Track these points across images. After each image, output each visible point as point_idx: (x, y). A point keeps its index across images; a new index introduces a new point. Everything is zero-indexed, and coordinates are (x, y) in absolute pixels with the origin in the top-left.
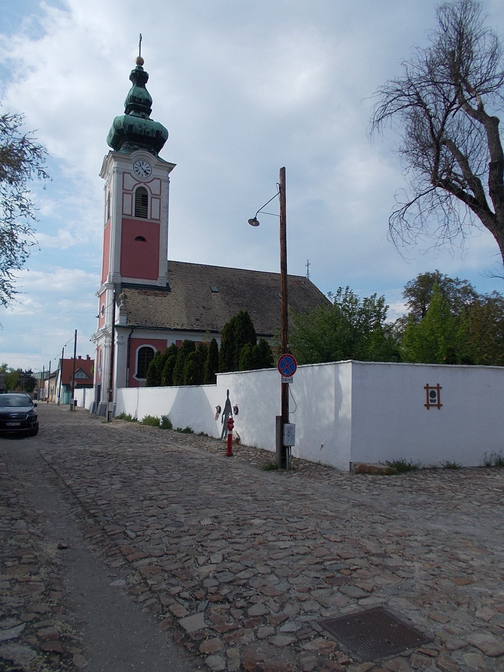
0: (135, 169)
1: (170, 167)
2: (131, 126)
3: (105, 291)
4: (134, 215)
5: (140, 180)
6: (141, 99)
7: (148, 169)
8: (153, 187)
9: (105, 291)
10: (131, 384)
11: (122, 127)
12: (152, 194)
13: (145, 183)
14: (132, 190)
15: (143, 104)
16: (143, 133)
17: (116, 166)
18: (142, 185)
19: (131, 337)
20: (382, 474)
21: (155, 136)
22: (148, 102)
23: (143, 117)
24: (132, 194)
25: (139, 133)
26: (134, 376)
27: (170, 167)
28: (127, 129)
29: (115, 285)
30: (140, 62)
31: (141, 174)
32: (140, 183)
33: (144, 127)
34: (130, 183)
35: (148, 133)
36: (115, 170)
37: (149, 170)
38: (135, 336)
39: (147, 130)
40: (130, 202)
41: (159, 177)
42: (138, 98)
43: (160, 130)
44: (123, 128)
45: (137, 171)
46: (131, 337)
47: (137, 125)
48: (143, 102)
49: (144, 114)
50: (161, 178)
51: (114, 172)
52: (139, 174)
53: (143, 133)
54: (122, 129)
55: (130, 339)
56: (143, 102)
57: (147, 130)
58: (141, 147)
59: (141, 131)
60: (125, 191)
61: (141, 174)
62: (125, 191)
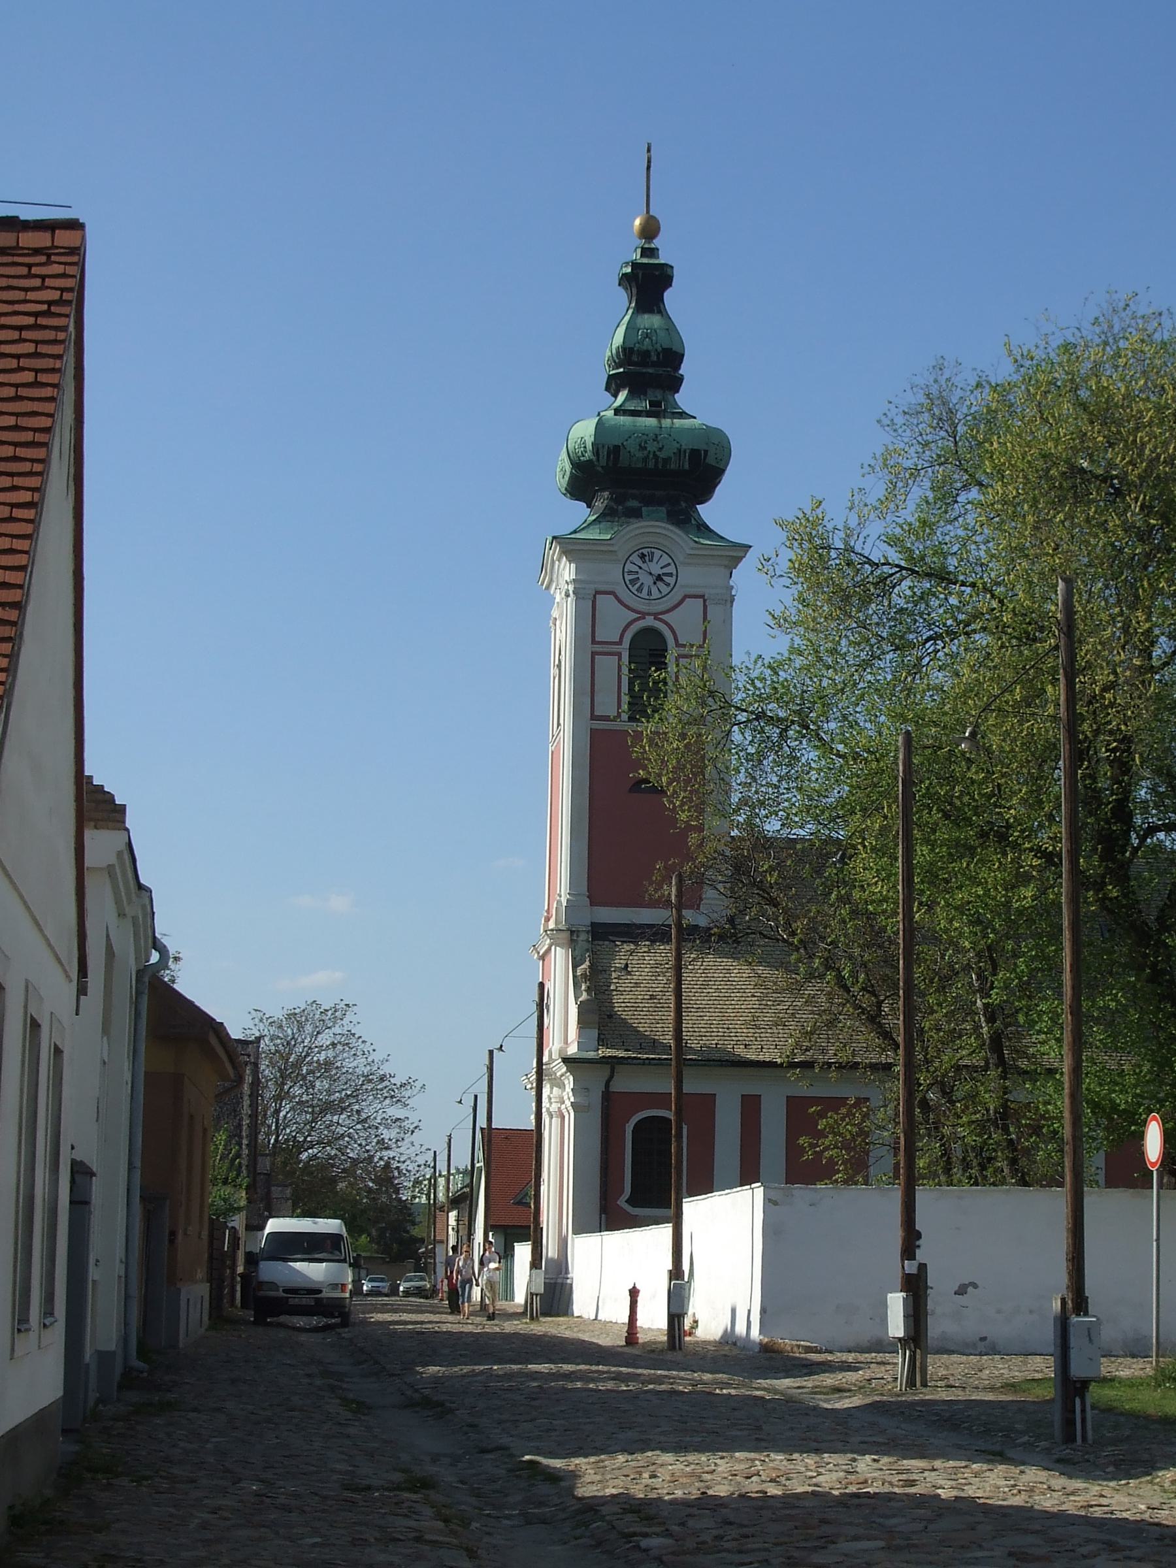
0: (628, 578)
1: (736, 552)
2: (615, 451)
3: (549, 949)
4: (625, 717)
5: (643, 608)
6: (647, 353)
7: (665, 570)
8: (684, 623)
9: (549, 949)
10: (581, 1228)
11: (588, 455)
12: (678, 645)
13: (656, 616)
14: (620, 643)
15: (654, 364)
16: (651, 465)
17: (573, 576)
18: (649, 621)
19: (613, 1089)
20: (211, 1243)
21: (687, 466)
22: (672, 358)
23: (656, 411)
24: (619, 655)
25: (640, 465)
26: (622, 1202)
27: (736, 552)
28: (603, 462)
29: (572, 932)
30: (650, 230)
31: (645, 591)
32: (643, 615)
33: (652, 447)
34: (615, 622)
35: (667, 460)
36: (571, 588)
37: (670, 575)
38: (622, 1084)
39: (662, 455)
40: (614, 671)
41: (699, 591)
42: (639, 352)
43: (703, 447)
44: (594, 458)
45: (633, 582)
46: (613, 1089)
47: (632, 445)
48: (654, 358)
49: (657, 395)
50: (708, 592)
51: (567, 595)
52: (640, 590)
53: (651, 465)
54: (590, 461)
55: (607, 1096)
56: (654, 358)
57: (662, 455)
58: (649, 501)
59: (645, 459)
60: (598, 648)
61: (645, 591)
62: (598, 648)
